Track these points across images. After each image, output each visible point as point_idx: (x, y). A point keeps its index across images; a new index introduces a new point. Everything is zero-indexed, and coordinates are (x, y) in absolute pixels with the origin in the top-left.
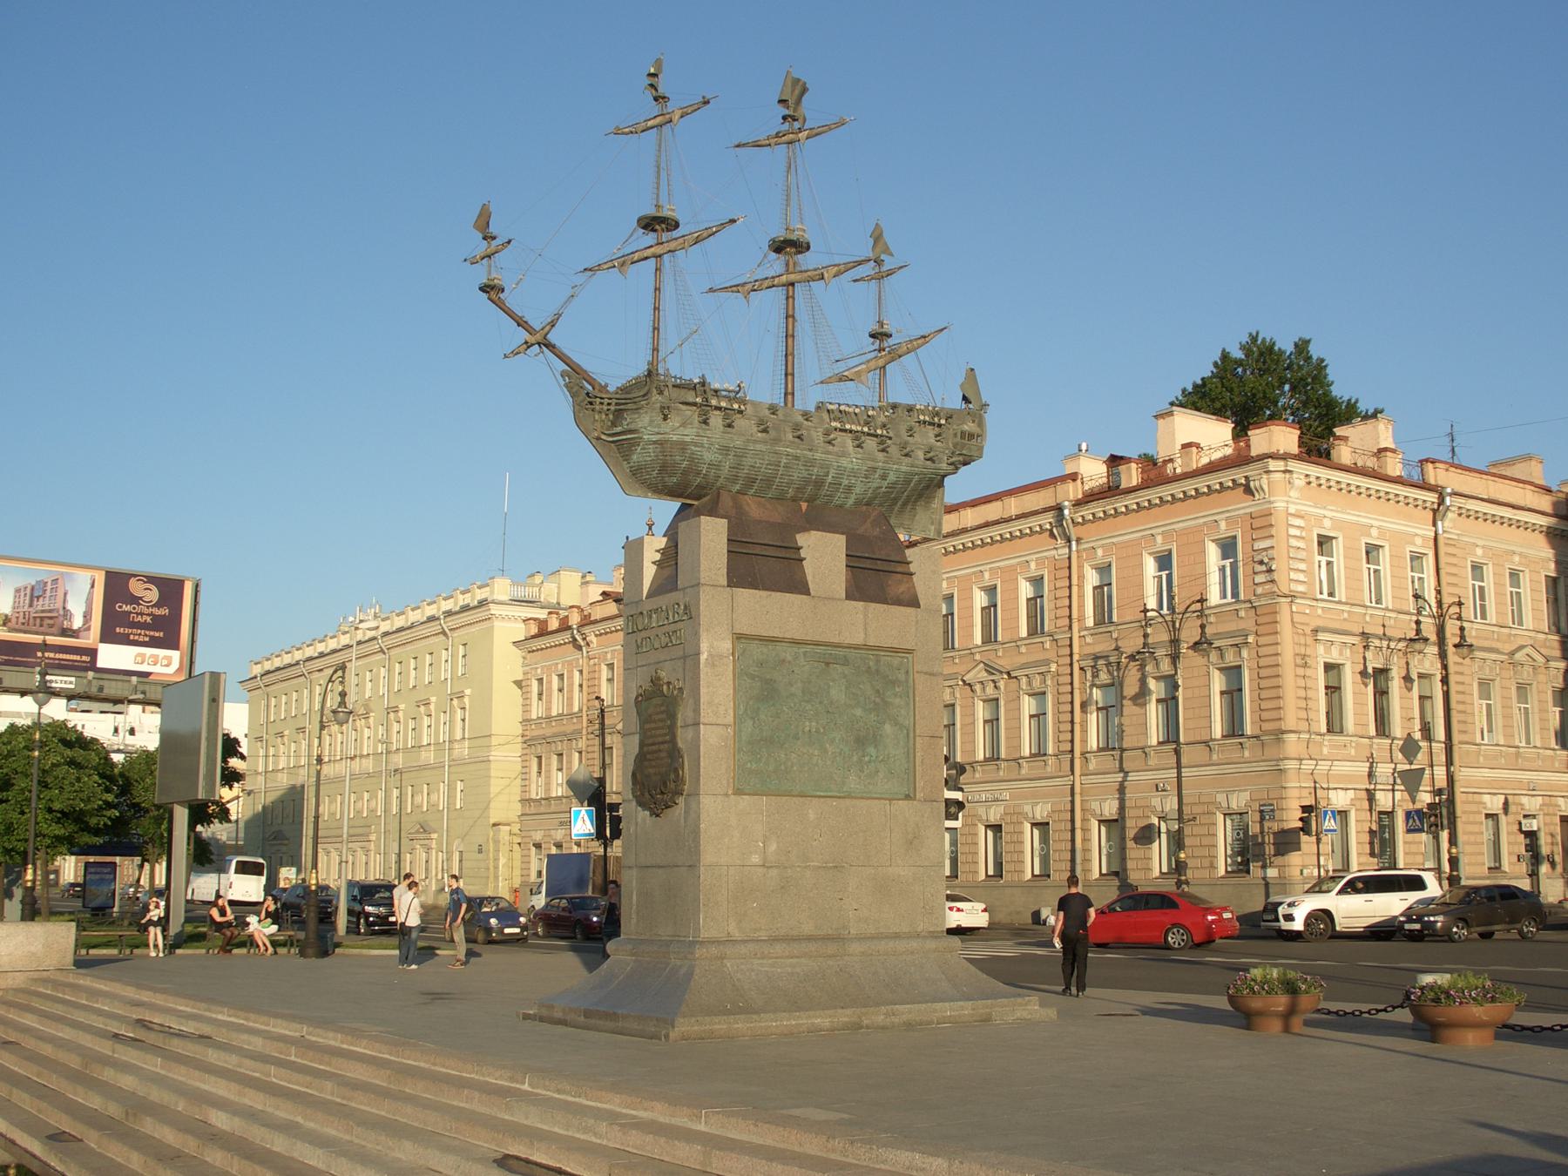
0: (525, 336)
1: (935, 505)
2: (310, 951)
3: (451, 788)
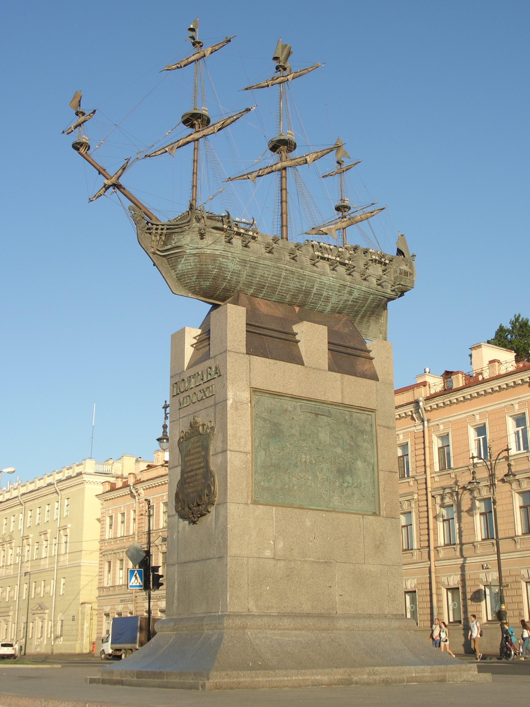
3: (57, 582)
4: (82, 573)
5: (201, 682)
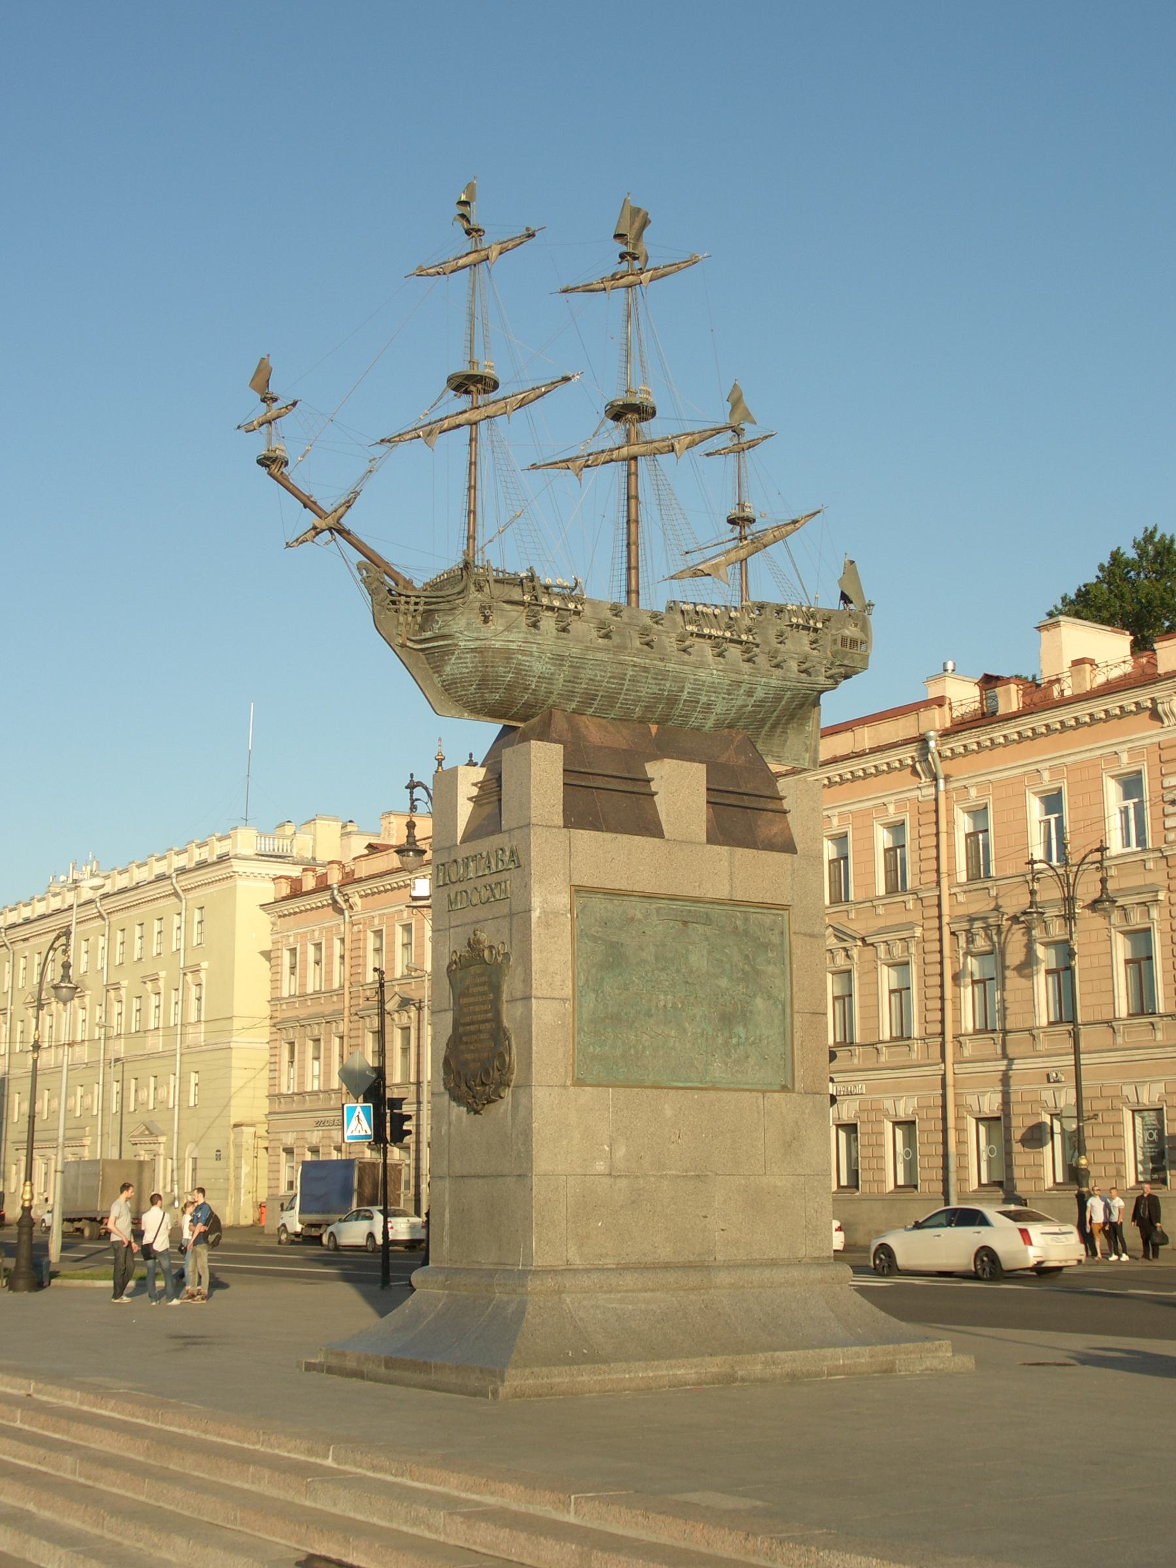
0: (314, 520)
1: (809, 728)
2: (21, 1283)
3: (183, 1080)
4: (234, 1063)
5: (490, 1388)
